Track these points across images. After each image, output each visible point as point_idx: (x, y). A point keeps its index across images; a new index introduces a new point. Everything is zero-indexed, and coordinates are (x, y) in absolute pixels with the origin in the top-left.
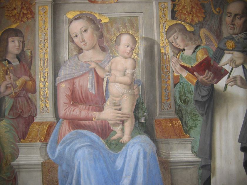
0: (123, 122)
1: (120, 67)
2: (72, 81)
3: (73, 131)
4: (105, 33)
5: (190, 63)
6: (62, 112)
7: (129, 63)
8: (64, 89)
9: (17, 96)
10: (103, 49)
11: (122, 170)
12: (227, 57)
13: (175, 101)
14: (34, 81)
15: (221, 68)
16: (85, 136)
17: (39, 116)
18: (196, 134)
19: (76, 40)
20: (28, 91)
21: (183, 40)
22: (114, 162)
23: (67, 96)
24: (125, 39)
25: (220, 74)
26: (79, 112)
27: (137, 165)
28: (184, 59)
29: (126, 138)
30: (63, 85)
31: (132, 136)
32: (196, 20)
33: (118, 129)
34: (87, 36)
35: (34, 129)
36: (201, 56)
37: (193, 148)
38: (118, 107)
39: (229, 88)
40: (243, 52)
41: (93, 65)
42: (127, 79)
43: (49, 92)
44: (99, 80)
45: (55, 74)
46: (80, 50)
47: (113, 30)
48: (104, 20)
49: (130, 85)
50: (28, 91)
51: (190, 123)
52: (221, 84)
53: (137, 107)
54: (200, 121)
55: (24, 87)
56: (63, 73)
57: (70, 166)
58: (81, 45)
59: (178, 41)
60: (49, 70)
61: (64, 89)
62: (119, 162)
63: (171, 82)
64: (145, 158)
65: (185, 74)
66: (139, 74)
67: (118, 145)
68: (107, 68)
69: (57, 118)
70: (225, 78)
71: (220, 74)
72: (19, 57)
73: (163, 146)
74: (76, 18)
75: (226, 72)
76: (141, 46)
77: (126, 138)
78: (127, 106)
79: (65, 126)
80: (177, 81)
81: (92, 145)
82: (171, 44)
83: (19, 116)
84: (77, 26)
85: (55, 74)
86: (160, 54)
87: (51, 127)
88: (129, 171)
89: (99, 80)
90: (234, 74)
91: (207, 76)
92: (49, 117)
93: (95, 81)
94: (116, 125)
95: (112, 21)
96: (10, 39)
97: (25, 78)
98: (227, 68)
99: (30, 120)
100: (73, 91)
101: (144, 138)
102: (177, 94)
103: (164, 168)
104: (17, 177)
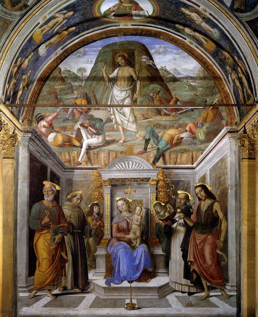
0: (136, 239)
1: (136, 219)
2: (118, 224)
3: (118, 242)
4: (131, 206)
5: (163, 218)
6: (114, 235)
7: (139, 217)
8: (115, 226)
9: (97, 229)
10: (130, 212)
11: (136, 257)
12: (177, 215)
13: (143, 153)
14: (104, 223)
15: (175, 220)
16: (122, 244)
17: (105, 236)
18: (164, 244)
19: (120, 208)
20: (101, 227)
21: (160, 209)
22: (133, 254)
23: (116, 229)
24: (138, 208)
25: (174, 221)
26: (119, 235)
27: (141, 255)
28: (160, 216)
29: (137, 245)
30: (114, 225)
31: (140, 245)
32: (165, 201)
33: (134, 242)
34: (124, 207)
35: (103, 241)
36: (167, 214)
37: (162, 249)
38: (135, 233)
39: (177, 227)
40: (184, 213)
41: (126, 218)
42: (138, 223)
43: (109, 227)
44: (128, 223)
45: (112, 221)
46: (121, 212)
47: (133, 205)
48: (130, 201)
49: (140, 225)
50: (101, 227)
51: (162, 240)
52: (175, 225)
53: (142, 234)
54: (166, 240)
55: (100, 225)
56: (114, 220)
57: (116, 255)
58: (122, 210)
59: (158, 209)
60: (109, 219)
61: (115, 226)
62: (135, 254)
63: (155, 225)
64: (145, 253)
65: (160, 222)
66: (144, 223)
67: (134, 248)
68: (131, 219)
69: (112, 236)
70: (176, 223)
71: (174, 221)
72: (98, 214)
73: (151, 248)
74: (120, 200)
75: (176, 221)
76: (144, 211)
77: (137, 245)
78: (138, 233)
79: (114, 240)
80: (157, 224)
81: (125, 248)
82: (155, 210)
83: (98, 236)
84: (120, 203)
85: (112, 221)
86: (151, 214)
87: (110, 241)
88: (139, 257)
89: (128, 223)
90: (180, 222)
91: (169, 222)
92: (109, 237)
93: (126, 224)
94: (134, 240)
95: (134, 201)
96: (94, 207)
97: (100, 222)
98: (177, 219)
99: (102, 238)
100: (118, 227)
101: (144, 246)
102: (157, 229)
103: (152, 257)
104: (28, 163)
